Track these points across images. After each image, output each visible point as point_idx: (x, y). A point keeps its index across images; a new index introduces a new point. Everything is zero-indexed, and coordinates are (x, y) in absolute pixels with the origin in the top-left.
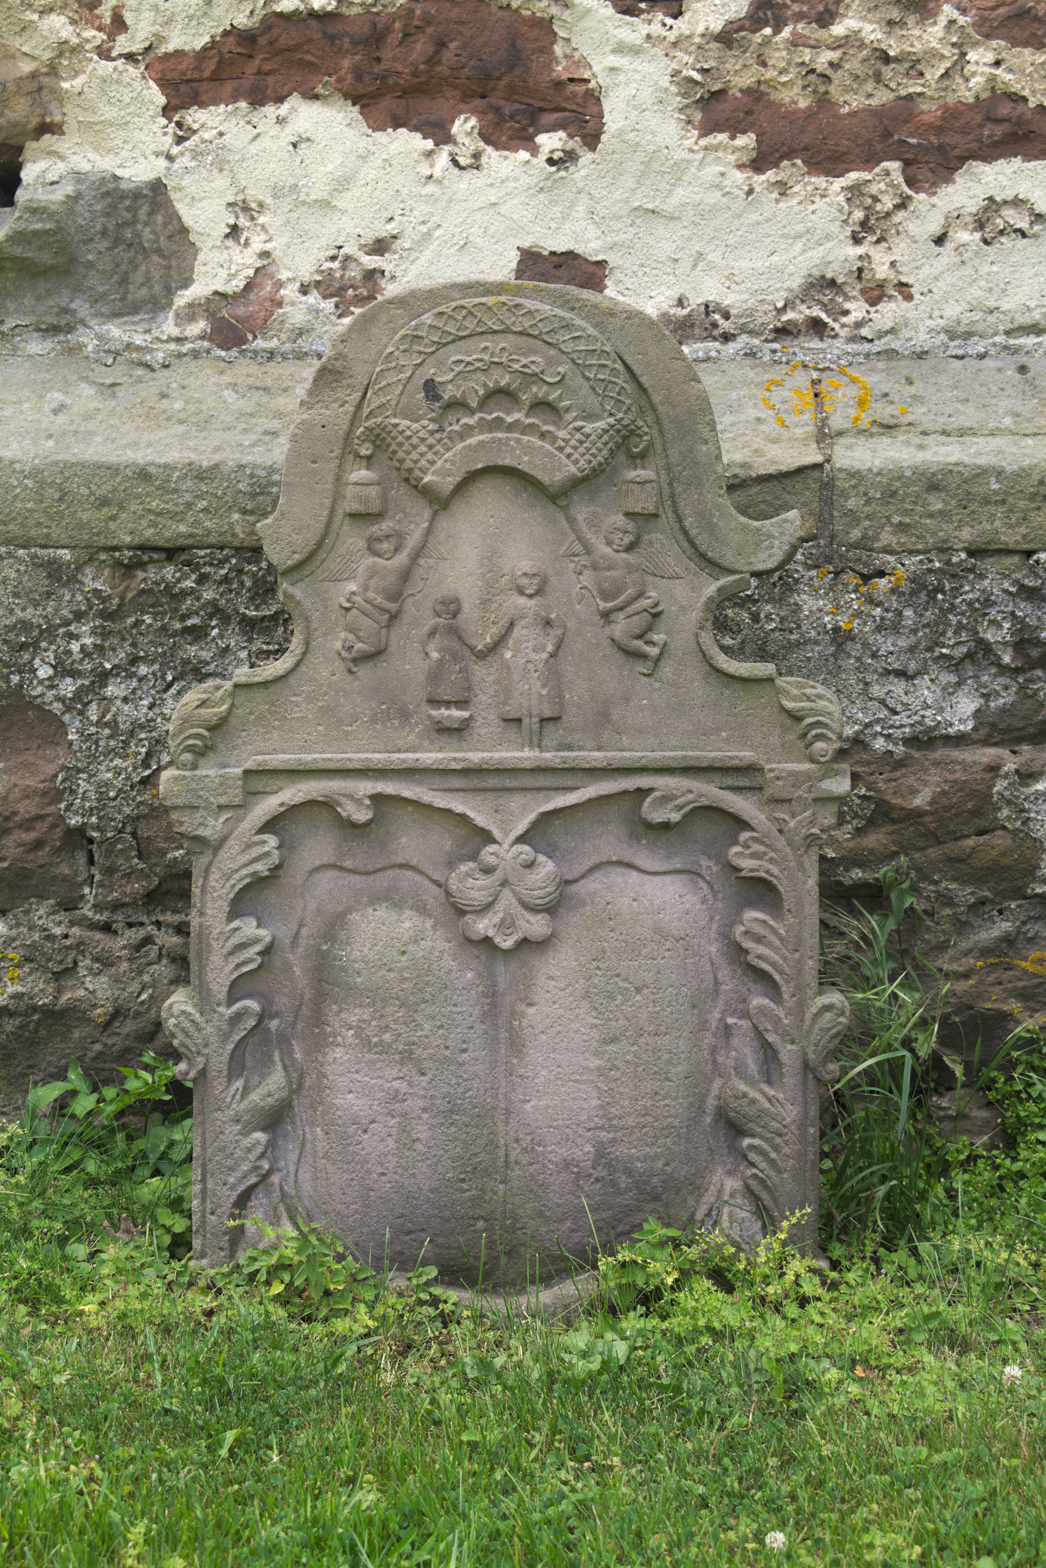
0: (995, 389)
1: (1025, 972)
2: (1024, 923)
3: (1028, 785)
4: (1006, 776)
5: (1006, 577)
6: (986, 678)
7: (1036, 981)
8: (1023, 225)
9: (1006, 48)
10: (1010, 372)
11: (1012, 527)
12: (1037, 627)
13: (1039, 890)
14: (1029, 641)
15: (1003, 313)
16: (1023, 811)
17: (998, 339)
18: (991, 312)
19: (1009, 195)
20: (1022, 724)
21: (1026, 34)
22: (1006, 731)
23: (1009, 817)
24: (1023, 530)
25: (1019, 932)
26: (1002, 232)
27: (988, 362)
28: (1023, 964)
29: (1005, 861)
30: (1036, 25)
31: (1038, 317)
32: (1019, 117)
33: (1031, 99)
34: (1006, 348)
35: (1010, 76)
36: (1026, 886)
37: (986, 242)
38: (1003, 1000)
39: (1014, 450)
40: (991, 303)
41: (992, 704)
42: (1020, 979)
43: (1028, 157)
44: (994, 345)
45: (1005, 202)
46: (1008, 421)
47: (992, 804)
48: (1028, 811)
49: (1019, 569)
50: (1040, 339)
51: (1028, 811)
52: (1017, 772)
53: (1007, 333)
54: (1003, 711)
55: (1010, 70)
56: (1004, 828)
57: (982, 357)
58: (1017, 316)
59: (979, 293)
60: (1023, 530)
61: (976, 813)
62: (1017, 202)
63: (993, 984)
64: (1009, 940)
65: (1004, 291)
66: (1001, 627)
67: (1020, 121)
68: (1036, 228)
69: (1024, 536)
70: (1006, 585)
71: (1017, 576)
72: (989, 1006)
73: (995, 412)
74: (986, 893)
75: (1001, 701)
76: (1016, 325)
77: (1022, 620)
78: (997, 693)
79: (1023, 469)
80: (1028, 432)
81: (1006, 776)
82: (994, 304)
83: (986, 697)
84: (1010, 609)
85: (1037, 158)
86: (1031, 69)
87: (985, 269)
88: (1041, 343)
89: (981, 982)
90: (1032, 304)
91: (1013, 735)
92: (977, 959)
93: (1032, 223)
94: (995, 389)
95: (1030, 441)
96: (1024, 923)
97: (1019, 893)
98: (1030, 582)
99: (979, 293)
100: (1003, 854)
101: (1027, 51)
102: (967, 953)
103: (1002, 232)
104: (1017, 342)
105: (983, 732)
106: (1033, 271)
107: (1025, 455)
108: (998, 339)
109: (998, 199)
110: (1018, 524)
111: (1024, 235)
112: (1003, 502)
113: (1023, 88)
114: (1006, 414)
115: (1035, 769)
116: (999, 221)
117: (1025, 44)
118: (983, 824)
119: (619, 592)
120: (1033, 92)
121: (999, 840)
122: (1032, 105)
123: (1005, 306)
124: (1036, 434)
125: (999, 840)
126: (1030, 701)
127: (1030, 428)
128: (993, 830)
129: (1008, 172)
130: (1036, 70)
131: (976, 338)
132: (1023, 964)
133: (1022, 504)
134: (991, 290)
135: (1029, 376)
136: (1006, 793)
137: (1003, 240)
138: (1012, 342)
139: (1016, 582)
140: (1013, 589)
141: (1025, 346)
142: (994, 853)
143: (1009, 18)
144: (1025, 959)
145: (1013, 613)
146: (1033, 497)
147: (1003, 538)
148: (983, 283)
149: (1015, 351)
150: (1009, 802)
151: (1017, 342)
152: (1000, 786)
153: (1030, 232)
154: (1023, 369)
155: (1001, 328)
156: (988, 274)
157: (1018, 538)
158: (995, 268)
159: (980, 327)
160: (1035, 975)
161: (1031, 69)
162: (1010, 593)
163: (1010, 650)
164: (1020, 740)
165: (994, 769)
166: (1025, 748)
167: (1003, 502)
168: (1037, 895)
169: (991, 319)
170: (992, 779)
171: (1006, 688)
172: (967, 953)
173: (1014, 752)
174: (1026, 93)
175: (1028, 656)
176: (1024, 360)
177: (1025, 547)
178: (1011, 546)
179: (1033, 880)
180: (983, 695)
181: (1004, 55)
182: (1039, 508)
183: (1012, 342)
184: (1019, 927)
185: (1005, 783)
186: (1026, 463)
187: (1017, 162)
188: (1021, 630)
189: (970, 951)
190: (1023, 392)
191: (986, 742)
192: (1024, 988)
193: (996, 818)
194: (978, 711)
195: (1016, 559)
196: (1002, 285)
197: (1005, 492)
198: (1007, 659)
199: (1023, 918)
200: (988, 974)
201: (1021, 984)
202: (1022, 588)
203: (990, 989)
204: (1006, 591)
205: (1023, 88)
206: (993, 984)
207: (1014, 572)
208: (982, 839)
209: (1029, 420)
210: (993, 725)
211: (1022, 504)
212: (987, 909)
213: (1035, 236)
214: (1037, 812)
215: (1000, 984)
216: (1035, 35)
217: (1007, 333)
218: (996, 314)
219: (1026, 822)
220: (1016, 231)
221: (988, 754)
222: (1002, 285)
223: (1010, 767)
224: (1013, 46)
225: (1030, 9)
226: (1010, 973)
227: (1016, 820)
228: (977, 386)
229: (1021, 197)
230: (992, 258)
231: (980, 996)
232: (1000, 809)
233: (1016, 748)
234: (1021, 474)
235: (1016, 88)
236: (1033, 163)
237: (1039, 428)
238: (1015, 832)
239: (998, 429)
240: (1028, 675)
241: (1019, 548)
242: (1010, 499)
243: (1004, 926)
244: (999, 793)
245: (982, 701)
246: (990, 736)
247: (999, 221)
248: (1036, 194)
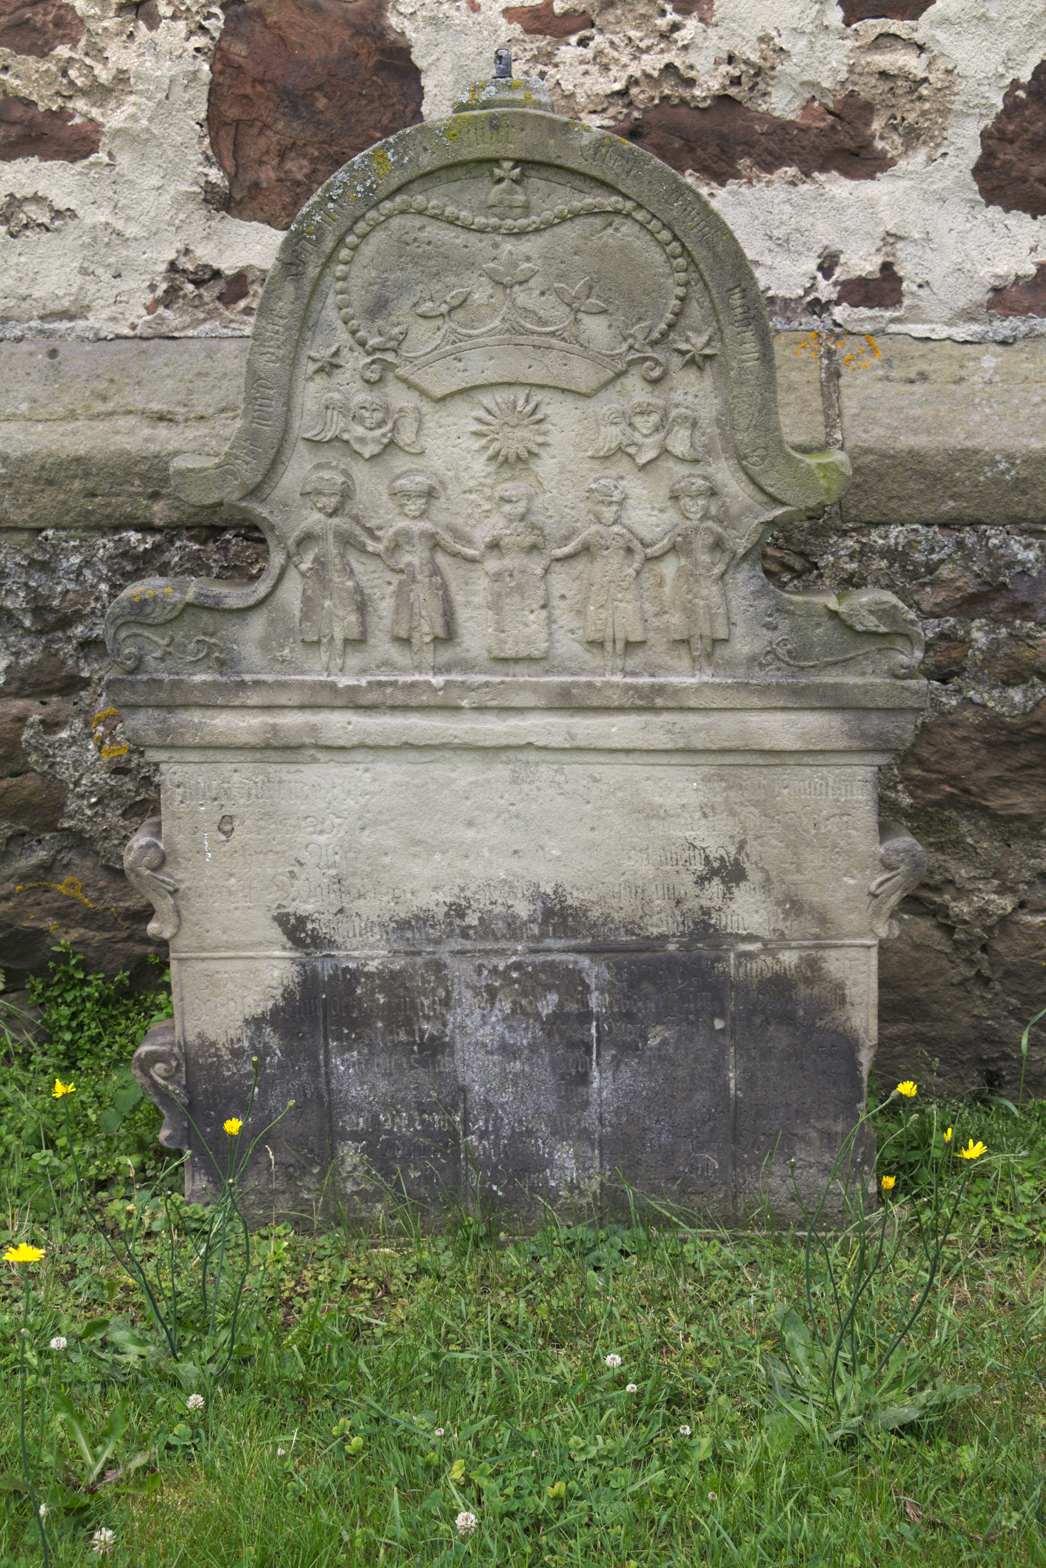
0: (21, 373)
1: (60, 894)
2: (58, 852)
3: (55, 733)
4: (32, 726)
5: (19, 551)
6: (12, 639)
7: (69, 902)
8: (45, 219)
9: (11, 55)
10: (40, 356)
11: (19, 507)
12: (49, 596)
13: (66, 825)
14: (44, 608)
15: (35, 300)
16: (48, 756)
17: (33, 324)
18: (24, 299)
19: (28, 192)
20: (48, 679)
21: (28, 43)
22: (36, 684)
23: (37, 762)
24: (29, 510)
25: (54, 860)
26: (26, 226)
27: (24, 346)
28: (60, 887)
29: (36, 800)
30: (35, 35)
31: (67, 304)
32: (31, 120)
33: (40, 104)
34: (41, 332)
35: (17, 82)
36: (56, 820)
37: (12, 235)
38: (41, 919)
39: (21, 437)
40: (23, 291)
41: (22, 662)
42: (56, 901)
43: (45, 158)
44: (30, 329)
45: (26, 199)
46: (24, 407)
47: (22, 750)
48: (54, 756)
49: (29, 544)
50: (72, 324)
51: (54, 756)
52: (42, 722)
53: (42, 318)
54: (31, 667)
55: (17, 76)
56: (34, 770)
57: (19, 340)
58: (48, 303)
59: (11, 282)
60: (29, 510)
61: (8, 758)
62: (37, 199)
63: (32, 905)
64: (46, 868)
65: (34, 280)
66: (18, 596)
67: (31, 124)
68: (57, 223)
69: (31, 516)
70: (18, 559)
71: (26, 551)
72: (26, 924)
73: (15, 398)
74: (22, 827)
75: (30, 658)
76: (48, 311)
77: (35, 590)
78: (25, 651)
79: (26, 456)
80: (40, 417)
81: (32, 726)
82: (25, 292)
83: (16, 654)
84: (23, 580)
85: (52, 158)
86: (36, 76)
87: (14, 260)
88: (73, 328)
89: (20, 904)
90: (60, 293)
91: (43, 688)
92: (17, 883)
93: (52, 219)
94: (21, 373)
95: (40, 427)
96: (58, 852)
97: (51, 827)
98: (38, 556)
99: (11, 282)
100: (33, 794)
101: (31, 59)
102: (9, 878)
103: (26, 226)
104: (52, 326)
105: (15, 685)
106: (59, 262)
107: (30, 442)
108: (33, 324)
109: (18, 196)
110: (25, 505)
111: (48, 230)
112: (10, 485)
113: (31, 93)
114: (24, 400)
115: (61, 719)
116: (21, 215)
117: (29, 52)
118: (16, 767)
119: (545, 324)
120: (41, 97)
121: (30, 782)
122: (42, 110)
123: (36, 294)
124: (47, 420)
125: (30, 782)
126: (54, 659)
127: (43, 413)
128: (26, 772)
129: (26, 170)
130: (41, 77)
131: (13, 323)
132: (60, 887)
133: (27, 487)
134: (21, 279)
135: (56, 361)
136: (33, 741)
137: (28, 233)
138: (46, 326)
139: (26, 557)
140: (24, 563)
141: (59, 330)
142: (25, 793)
143: (9, 27)
144: (60, 883)
145: (26, 584)
146: (36, 481)
147: (12, 517)
148: (13, 273)
149: (50, 334)
150: (36, 749)
151: (52, 326)
152: (27, 734)
153: (52, 227)
154: (53, 353)
155: (35, 313)
156: (17, 264)
157: (26, 517)
158: (23, 259)
159: (15, 313)
160: (68, 897)
161: (36, 76)
162: (23, 566)
163: (29, 615)
164: (50, 693)
165: (21, 720)
166: (55, 699)
167: (10, 485)
168: (64, 829)
169: (25, 305)
170: (20, 728)
171: (33, 647)
172: (9, 878)
173: (43, 703)
174: (34, 98)
175: (45, 620)
176: (54, 343)
177: (33, 525)
178: (20, 525)
179: (62, 816)
180: (13, 654)
181: (9, 61)
182: (43, 491)
183: (46, 326)
184: (55, 856)
185: (32, 732)
186: (30, 449)
187: (34, 161)
188: (35, 598)
189: (12, 876)
190: (47, 377)
191: (18, 695)
192: (59, 908)
193: (27, 762)
194: (9, 667)
195: (25, 536)
196: (31, 275)
197: (13, 477)
198: (27, 623)
199: (57, 848)
200: (27, 897)
201: (57, 904)
202: (33, 563)
203: (29, 910)
204: (18, 564)
205: (31, 93)
206: (32, 905)
207: (24, 547)
208: (14, 780)
209: (44, 406)
210: (23, 680)
211: (27, 487)
212: (26, 840)
213: (57, 230)
214: (63, 757)
215: (39, 904)
216: (36, 44)
217: (42, 318)
218: (28, 301)
219: (52, 765)
220: (39, 225)
221: (18, 705)
222: (31, 275)
223: (35, 718)
224: (18, 53)
225: (28, 20)
226: (49, 895)
227: (43, 764)
228: (7, 370)
229: (40, 194)
230: (19, 250)
231: (19, 916)
232: (29, 754)
233: (46, 700)
234: (24, 460)
235: (24, 92)
236: (49, 163)
237: (51, 414)
238: (44, 774)
239: (14, 415)
240: (50, 636)
241: (27, 526)
242: (16, 483)
243: (41, 854)
244: (26, 741)
245: (13, 658)
246: (21, 689)
247: (21, 215)
248: (54, 192)
